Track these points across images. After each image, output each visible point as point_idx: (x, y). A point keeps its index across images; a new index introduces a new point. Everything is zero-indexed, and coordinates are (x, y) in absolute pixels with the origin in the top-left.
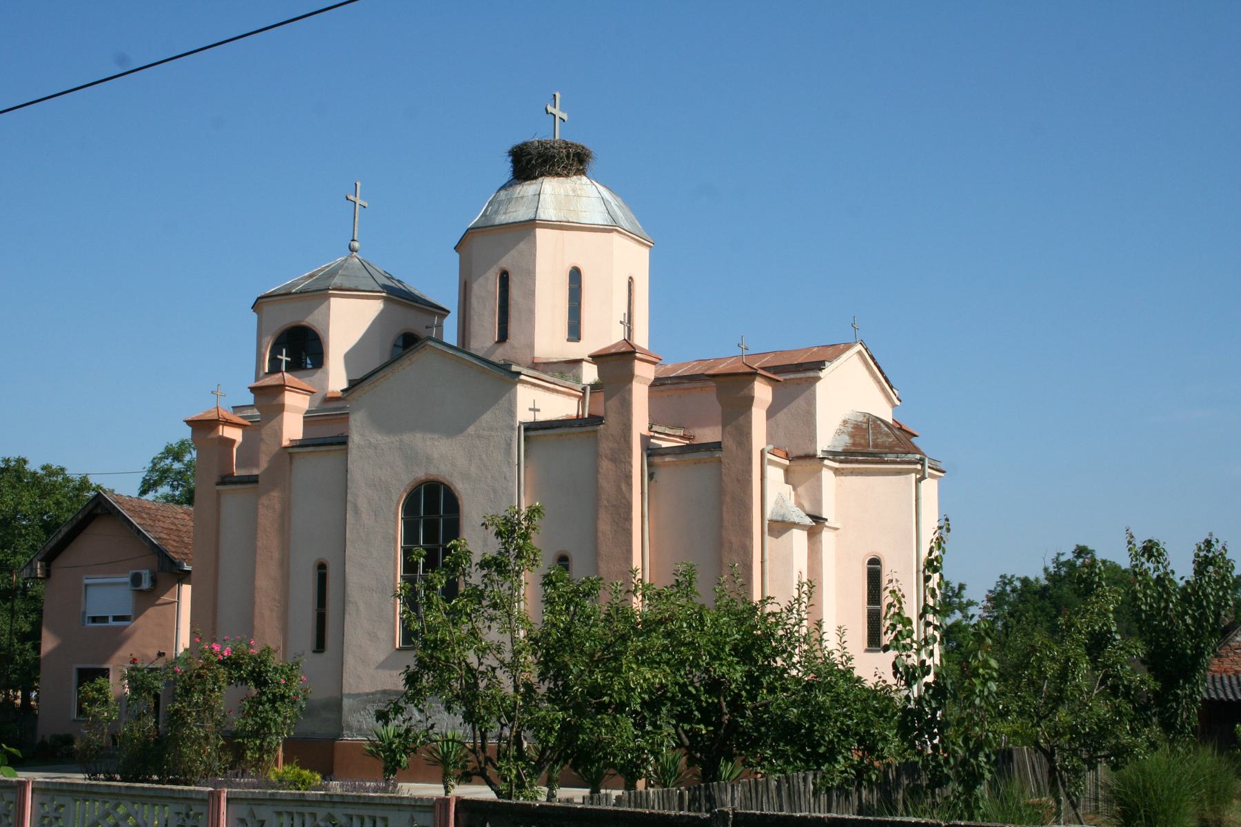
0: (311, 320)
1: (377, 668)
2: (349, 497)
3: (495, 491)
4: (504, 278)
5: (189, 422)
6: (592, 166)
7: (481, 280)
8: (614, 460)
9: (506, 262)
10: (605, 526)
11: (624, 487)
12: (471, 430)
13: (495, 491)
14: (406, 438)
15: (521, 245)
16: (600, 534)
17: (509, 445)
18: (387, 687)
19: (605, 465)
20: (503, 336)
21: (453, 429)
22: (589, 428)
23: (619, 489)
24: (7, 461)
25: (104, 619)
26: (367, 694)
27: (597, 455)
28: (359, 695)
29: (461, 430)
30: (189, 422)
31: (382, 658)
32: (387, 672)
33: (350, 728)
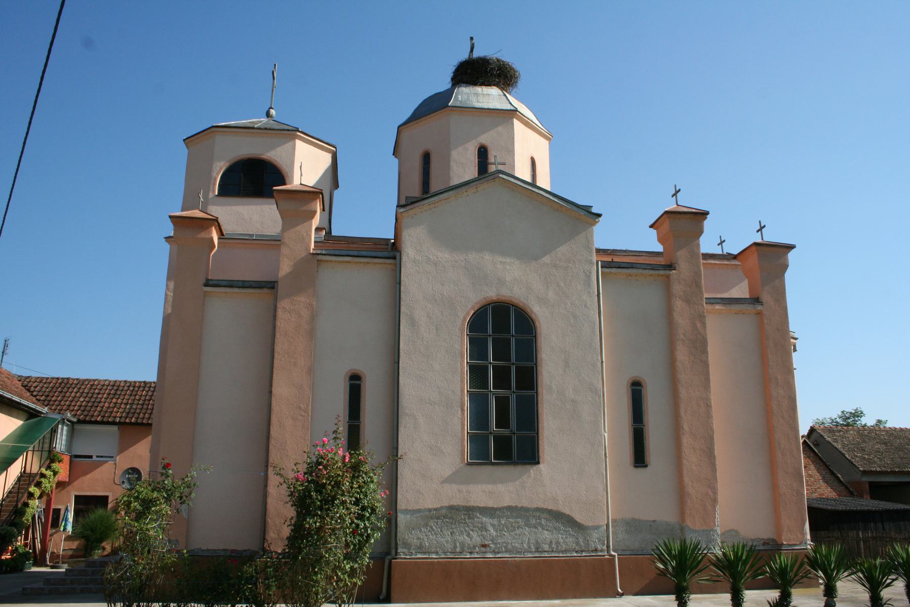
0: (275, 155)
1: (443, 482)
2: (403, 309)
5: (651, 226)
7: (460, 149)
8: (687, 301)
9: (484, 139)
10: (682, 355)
11: (698, 325)
12: (547, 259)
14: (473, 257)
15: (500, 128)
16: (678, 363)
17: (589, 277)
18: (455, 502)
19: (678, 304)
21: (527, 255)
22: (662, 272)
25: (91, 457)
26: (430, 510)
28: (419, 511)
29: (536, 258)
30: (651, 226)
31: (448, 472)
32: (455, 486)
33: (407, 545)
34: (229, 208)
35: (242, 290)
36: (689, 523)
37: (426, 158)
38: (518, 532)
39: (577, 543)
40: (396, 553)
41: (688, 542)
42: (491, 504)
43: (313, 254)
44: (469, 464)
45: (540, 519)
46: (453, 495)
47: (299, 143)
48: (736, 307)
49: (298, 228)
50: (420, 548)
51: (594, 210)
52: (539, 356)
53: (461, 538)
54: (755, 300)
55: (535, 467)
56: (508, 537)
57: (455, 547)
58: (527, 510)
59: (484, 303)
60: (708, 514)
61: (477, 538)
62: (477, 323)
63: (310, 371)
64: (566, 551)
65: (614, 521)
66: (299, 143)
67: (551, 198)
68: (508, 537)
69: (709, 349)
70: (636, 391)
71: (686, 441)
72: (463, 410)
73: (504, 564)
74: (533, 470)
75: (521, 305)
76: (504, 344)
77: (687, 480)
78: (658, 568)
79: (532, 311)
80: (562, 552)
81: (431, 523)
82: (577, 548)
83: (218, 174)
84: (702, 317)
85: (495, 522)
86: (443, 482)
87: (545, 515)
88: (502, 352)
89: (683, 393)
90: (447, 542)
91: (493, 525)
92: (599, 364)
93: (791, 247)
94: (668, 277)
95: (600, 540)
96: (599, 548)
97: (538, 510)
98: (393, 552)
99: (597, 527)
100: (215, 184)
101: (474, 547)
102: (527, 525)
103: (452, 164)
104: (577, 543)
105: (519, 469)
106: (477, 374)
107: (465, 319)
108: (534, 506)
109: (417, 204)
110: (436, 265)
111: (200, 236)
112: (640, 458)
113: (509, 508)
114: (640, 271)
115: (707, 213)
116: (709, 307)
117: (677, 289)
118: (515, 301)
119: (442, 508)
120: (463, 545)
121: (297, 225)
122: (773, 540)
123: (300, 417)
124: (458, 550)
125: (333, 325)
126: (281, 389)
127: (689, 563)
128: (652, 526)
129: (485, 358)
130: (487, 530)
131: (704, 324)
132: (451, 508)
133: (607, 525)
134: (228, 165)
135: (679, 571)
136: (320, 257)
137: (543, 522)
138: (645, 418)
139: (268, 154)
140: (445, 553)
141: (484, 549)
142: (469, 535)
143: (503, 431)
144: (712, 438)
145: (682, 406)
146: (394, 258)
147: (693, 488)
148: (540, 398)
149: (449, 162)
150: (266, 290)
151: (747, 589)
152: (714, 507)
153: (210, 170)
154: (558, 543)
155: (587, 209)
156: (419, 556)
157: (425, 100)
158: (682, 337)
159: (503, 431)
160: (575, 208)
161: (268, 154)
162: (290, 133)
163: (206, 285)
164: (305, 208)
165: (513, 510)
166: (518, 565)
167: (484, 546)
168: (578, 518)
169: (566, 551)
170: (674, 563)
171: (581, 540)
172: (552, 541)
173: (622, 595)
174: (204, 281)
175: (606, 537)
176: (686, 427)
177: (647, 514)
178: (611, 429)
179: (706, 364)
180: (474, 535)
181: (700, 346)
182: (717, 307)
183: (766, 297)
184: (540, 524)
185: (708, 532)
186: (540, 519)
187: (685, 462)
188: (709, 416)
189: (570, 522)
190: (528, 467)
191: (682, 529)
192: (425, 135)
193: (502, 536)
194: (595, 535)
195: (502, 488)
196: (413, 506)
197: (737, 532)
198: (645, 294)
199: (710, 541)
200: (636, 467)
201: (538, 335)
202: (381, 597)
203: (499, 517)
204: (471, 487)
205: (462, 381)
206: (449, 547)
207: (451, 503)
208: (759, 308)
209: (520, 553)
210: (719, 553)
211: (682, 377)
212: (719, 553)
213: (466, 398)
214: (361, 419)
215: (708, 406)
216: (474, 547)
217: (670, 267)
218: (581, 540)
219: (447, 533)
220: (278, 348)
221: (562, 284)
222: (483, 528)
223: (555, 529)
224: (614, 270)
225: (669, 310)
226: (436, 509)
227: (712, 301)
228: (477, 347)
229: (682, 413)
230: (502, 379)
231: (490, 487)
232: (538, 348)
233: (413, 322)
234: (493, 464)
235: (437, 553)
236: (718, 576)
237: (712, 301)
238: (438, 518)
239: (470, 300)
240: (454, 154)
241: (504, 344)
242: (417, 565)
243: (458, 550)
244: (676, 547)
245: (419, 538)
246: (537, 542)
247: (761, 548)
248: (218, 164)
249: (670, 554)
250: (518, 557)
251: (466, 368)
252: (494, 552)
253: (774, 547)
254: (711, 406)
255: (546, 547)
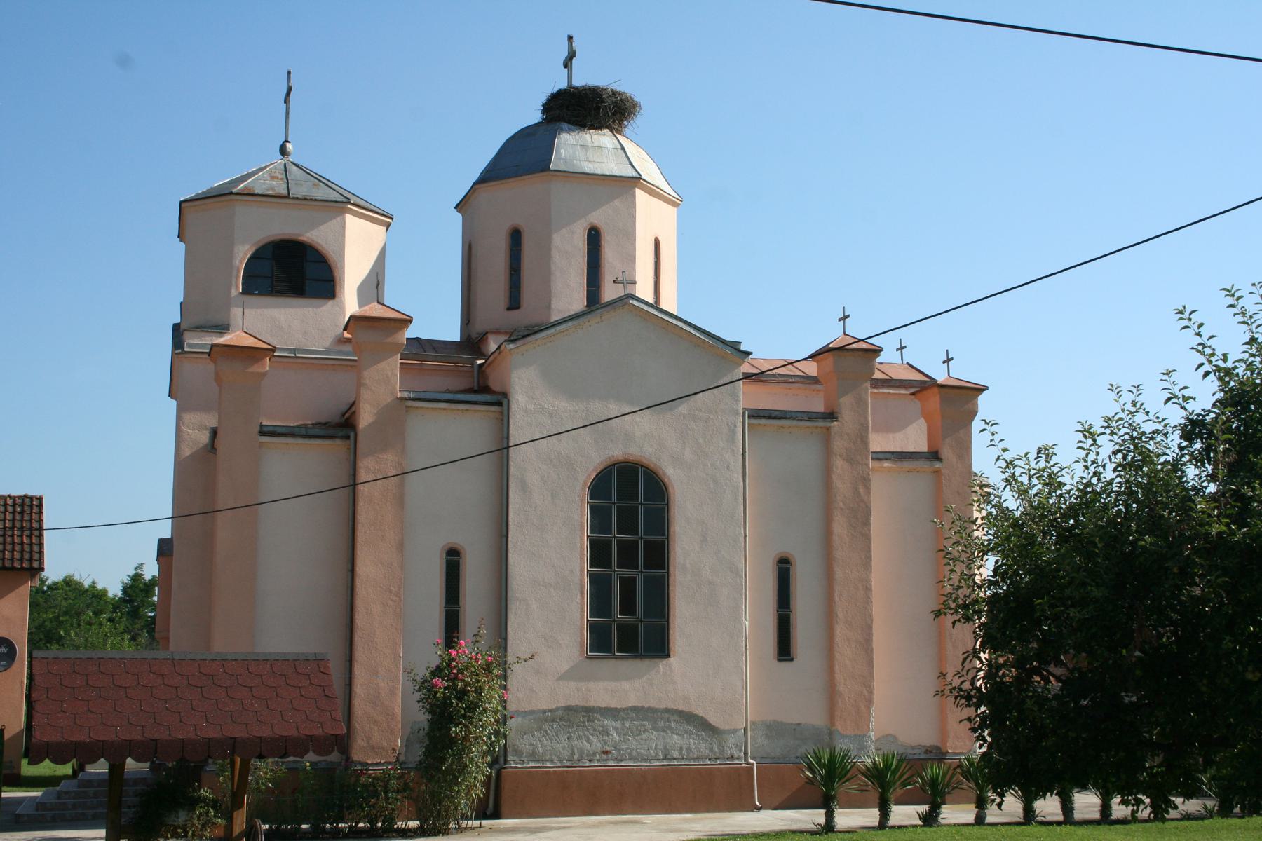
0: (317, 236)
1: (559, 679)
2: (512, 470)
3: (715, 481)
4: (594, 237)
6: (636, 125)
8: (850, 460)
9: (597, 218)
10: (840, 527)
11: (861, 490)
13: (715, 481)
15: (617, 202)
16: (835, 538)
17: (733, 431)
18: (572, 702)
19: (839, 464)
20: (514, 303)
22: (821, 424)
23: (856, 490)
24: (431, 370)
26: (544, 712)
27: (828, 453)
28: (532, 712)
31: (565, 667)
32: (573, 684)
33: (518, 752)
34: (259, 311)
35: (307, 441)
36: (839, 727)
37: (516, 236)
38: (644, 736)
39: (711, 750)
40: (506, 762)
41: (837, 749)
42: (614, 704)
43: (401, 399)
44: (589, 658)
45: (669, 720)
46: (571, 694)
47: (348, 217)
48: (907, 465)
49: (381, 365)
50: (533, 756)
51: (743, 348)
52: (672, 529)
53: (579, 744)
54: (934, 455)
55: (665, 661)
56: (633, 743)
57: (573, 754)
58: (654, 710)
59: (609, 463)
60: (861, 718)
61: (597, 744)
62: (599, 487)
63: (401, 546)
64: (698, 758)
65: (753, 723)
66: (348, 217)
67: (692, 331)
68: (633, 743)
69: (873, 520)
70: (784, 569)
71: (839, 630)
72: (582, 593)
73: (629, 773)
74: (662, 665)
75: (652, 466)
76: (630, 513)
77: (838, 676)
78: (808, 777)
79: (664, 474)
80: (694, 759)
81: (546, 726)
82: (711, 755)
83: (241, 262)
84: (866, 481)
85: (618, 724)
86: (559, 679)
87: (675, 717)
88: (627, 524)
89: (839, 573)
90: (564, 748)
91: (616, 729)
92: (742, 539)
93: (981, 389)
94: (828, 429)
95: (736, 746)
96: (736, 755)
97: (667, 711)
98: (502, 760)
99: (734, 731)
100: (238, 276)
101: (595, 754)
102: (654, 728)
103: (556, 255)
104: (711, 750)
105: (647, 662)
106: (599, 553)
107: (585, 483)
108: (663, 706)
109: (529, 339)
110: (551, 415)
111: (251, 370)
112: (785, 650)
113: (634, 709)
114: (795, 422)
115: (881, 350)
116: (876, 464)
117: (839, 444)
118: (645, 462)
119: (557, 709)
120: (581, 751)
121: (380, 361)
122: (938, 748)
123: (391, 603)
124: (576, 757)
125: (425, 483)
126: (366, 567)
127: (838, 771)
128: (796, 730)
129: (609, 531)
130: (608, 735)
131: (868, 489)
132: (568, 709)
133: (746, 729)
134: (254, 249)
135: (824, 781)
136: (410, 403)
137: (673, 724)
138: (792, 603)
139: (308, 235)
140: (561, 761)
141: (604, 756)
142: (588, 740)
143: (628, 619)
144: (870, 628)
145: (837, 589)
146: (500, 404)
147: (845, 686)
148: (671, 579)
149: (550, 249)
150: (338, 442)
151: (897, 803)
152: (869, 709)
153: (230, 256)
154: (689, 749)
155: (734, 346)
156: (532, 764)
157: (508, 141)
158: (841, 505)
159: (628, 619)
160: (720, 345)
161: (308, 235)
162: (340, 204)
163: (262, 433)
164: (390, 340)
165: (640, 712)
166: (643, 774)
167: (606, 752)
168: (713, 720)
169: (698, 758)
170: (823, 772)
171: (715, 746)
172: (682, 747)
173: (761, 808)
174: (258, 429)
175: (744, 744)
176: (840, 615)
177: (792, 718)
178: (753, 617)
179: (867, 538)
180: (594, 740)
181: (861, 517)
182: (886, 464)
183: (946, 452)
184: (670, 728)
185: (861, 739)
186: (669, 720)
187: (837, 655)
188: (868, 600)
189: (704, 725)
190: (657, 660)
191: (831, 734)
192: (515, 198)
193: (626, 741)
194: (731, 740)
195: (626, 684)
196: (525, 707)
197: (895, 737)
198: (800, 450)
199: (862, 748)
200: (780, 660)
201: (671, 503)
202: (488, 813)
203: (623, 719)
204: (591, 685)
205: (582, 559)
206: (566, 754)
207: (569, 703)
208: (937, 465)
209: (645, 760)
210: (869, 761)
211: (839, 554)
212: (869, 761)
213: (586, 580)
214: (461, 604)
215: (868, 589)
216: (595, 754)
217: (831, 416)
218: (715, 746)
219: (564, 737)
220: (361, 518)
221: (701, 441)
222: (605, 732)
223: (686, 732)
224: (763, 421)
225: (827, 471)
226: (550, 711)
227: (880, 457)
228: (599, 518)
229: (837, 598)
230: (627, 556)
231: (612, 685)
232: (671, 520)
233: (525, 488)
234: (617, 658)
235: (552, 761)
236: (867, 785)
237: (881, 456)
238: (553, 721)
239: (592, 455)
240: (557, 239)
241: (630, 513)
242: (531, 775)
243: (576, 757)
244: (826, 756)
245: (531, 744)
246: (665, 748)
247: (922, 757)
248: (241, 248)
249: (819, 762)
250: (644, 766)
251: (586, 543)
252: (616, 759)
253: (937, 755)
254: (870, 590)
255: (676, 754)
